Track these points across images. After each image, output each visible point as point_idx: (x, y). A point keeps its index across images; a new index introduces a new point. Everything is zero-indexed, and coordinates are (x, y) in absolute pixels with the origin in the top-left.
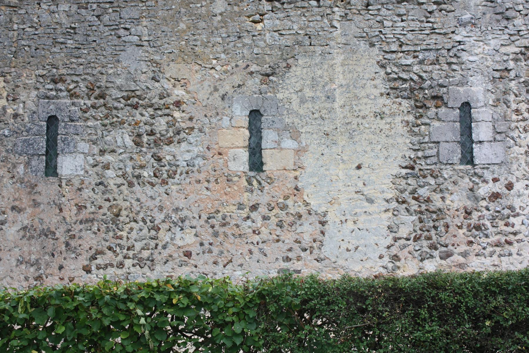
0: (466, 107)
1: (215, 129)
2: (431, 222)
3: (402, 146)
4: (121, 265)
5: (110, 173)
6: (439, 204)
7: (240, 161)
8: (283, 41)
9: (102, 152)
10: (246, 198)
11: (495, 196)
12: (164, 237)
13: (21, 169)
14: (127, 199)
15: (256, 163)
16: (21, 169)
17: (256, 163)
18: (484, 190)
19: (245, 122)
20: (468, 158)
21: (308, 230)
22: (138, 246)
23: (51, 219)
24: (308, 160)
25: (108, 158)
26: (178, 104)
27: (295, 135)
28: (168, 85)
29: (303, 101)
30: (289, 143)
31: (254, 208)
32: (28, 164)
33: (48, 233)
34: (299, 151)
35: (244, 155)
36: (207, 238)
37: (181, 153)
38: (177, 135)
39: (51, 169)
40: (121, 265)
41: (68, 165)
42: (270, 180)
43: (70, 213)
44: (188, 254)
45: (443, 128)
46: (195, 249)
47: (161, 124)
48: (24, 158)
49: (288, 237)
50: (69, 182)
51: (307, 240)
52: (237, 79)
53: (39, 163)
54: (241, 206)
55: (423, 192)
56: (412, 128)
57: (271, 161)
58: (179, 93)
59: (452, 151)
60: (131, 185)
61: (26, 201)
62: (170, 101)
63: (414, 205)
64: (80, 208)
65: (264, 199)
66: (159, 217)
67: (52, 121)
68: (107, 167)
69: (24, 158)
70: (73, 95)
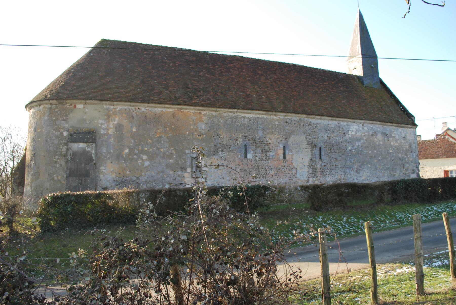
0: (320, 148)
1: (277, 149)
2: (314, 172)
3: (310, 156)
4: (260, 178)
5: (257, 158)
6: (315, 167)
7: (281, 157)
8: (289, 132)
9: (255, 153)
10: (283, 164)
11: (325, 166)
12: (268, 172)
13: (239, 156)
14: (261, 163)
15: (284, 157)
16: (239, 156)
17: (284, 157)
18: (323, 165)
19: (282, 149)
20: (320, 158)
21: (294, 172)
22: (263, 174)
23: (246, 168)
24: (294, 157)
25: (257, 154)
26: (270, 143)
27: (292, 152)
28: (268, 139)
29: (293, 144)
30: (291, 154)
31: (284, 166)
32: (241, 155)
33: (245, 170)
34: (292, 155)
35: (282, 156)
36: (276, 172)
37: (271, 154)
38: (270, 150)
39: (246, 157)
40: (260, 178)
41: (249, 156)
42: (287, 161)
43: (250, 166)
44: (272, 176)
45: (317, 151)
46: (274, 175)
47: (267, 148)
48: (240, 154)
49: (291, 172)
50: (249, 160)
51: (294, 173)
52: (281, 139)
53: (243, 155)
54: (282, 166)
55: (313, 164)
56: (311, 151)
57: (287, 157)
58: (270, 141)
59: (318, 157)
60: (261, 160)
61: (241, 163)
62: (268, 143)
63: (312, 167)
64: (252, 165)
65: (286, 165)
66: (267, 168)
67: (246, 145)
68: (256, 156)
69: (240, 154)
70: (249, 140)
